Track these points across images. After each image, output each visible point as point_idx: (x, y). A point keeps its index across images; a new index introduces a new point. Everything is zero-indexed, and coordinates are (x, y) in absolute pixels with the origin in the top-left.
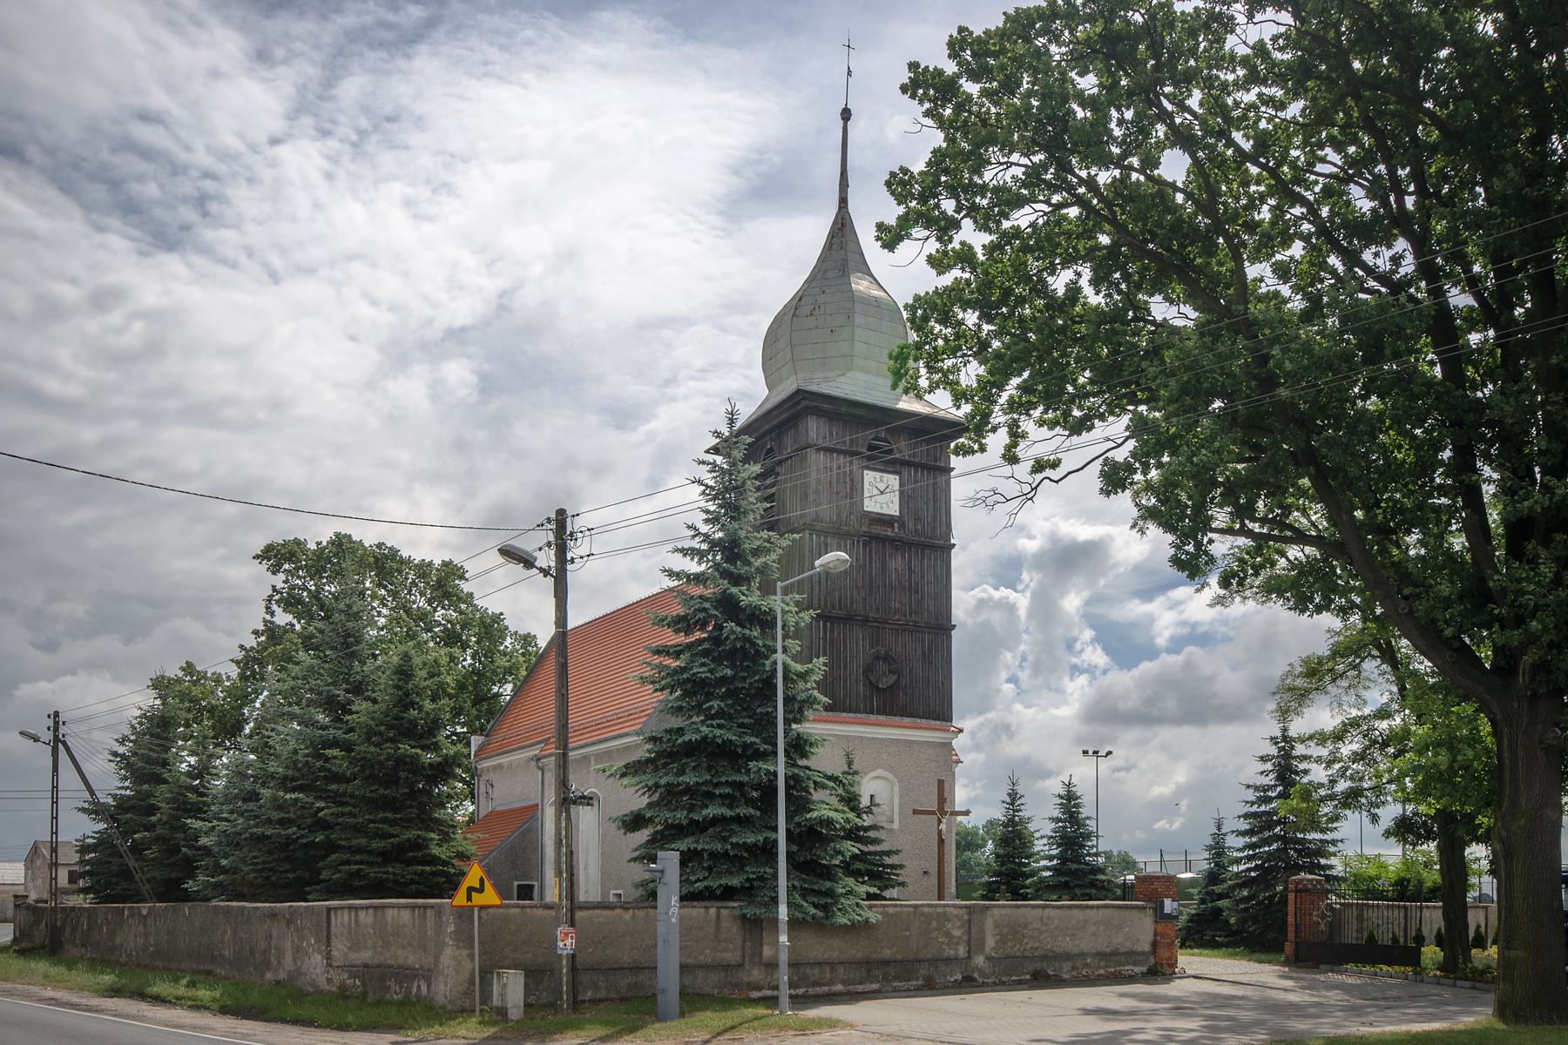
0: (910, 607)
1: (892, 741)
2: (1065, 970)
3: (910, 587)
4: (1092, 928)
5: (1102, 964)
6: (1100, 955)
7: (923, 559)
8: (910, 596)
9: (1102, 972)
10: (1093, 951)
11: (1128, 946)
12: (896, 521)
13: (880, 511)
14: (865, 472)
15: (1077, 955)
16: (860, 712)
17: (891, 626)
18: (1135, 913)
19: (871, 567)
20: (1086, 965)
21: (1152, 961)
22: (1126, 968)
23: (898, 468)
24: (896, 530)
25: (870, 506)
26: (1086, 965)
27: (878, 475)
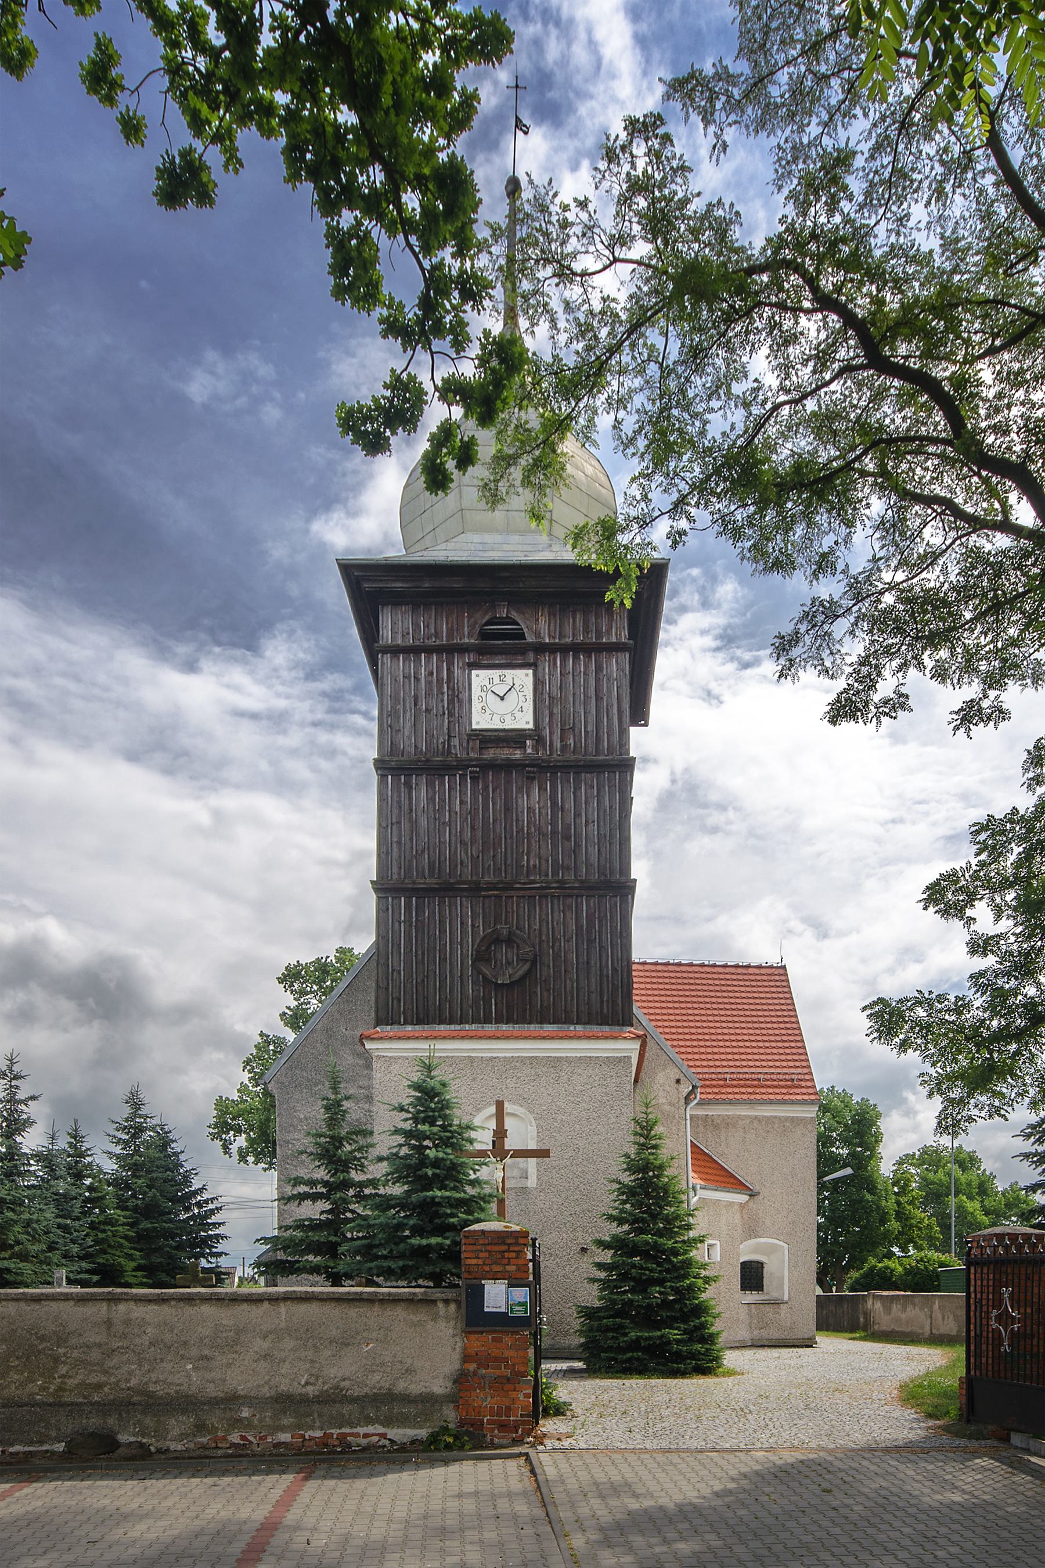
0: (555, 861)
1: (522, 1060)
2: (176, 1432)
3: (554, 832)
4: (262, 1345)
5: (285, 1421)
6: (285, 1402)
7: (577, 788)
8: (555, 846)
9: (285, 1437)
10: (266, 1392)
11: (377, 1381)
12: (530, 737)
13: (501, 726)
14: (474, 672)
15: (214, 1402)
16: (467, 1022)
17: (521, 893)
18: (400, 1312)
19: (486, 808)
20: (237, 1423)
21: (450, 1415)
22: (361, 1430)
23: (531, 657)
24: (529, 751)
25: (481, 720)
26: (237, 1423)
27: (495, 674)
